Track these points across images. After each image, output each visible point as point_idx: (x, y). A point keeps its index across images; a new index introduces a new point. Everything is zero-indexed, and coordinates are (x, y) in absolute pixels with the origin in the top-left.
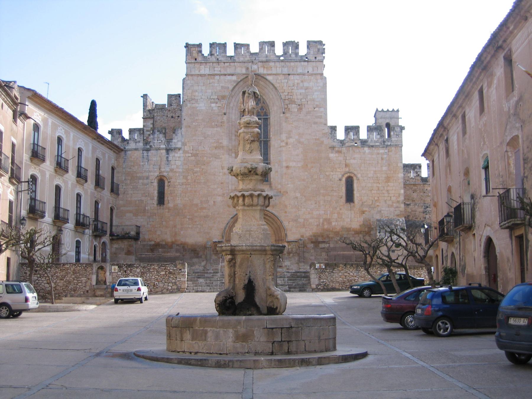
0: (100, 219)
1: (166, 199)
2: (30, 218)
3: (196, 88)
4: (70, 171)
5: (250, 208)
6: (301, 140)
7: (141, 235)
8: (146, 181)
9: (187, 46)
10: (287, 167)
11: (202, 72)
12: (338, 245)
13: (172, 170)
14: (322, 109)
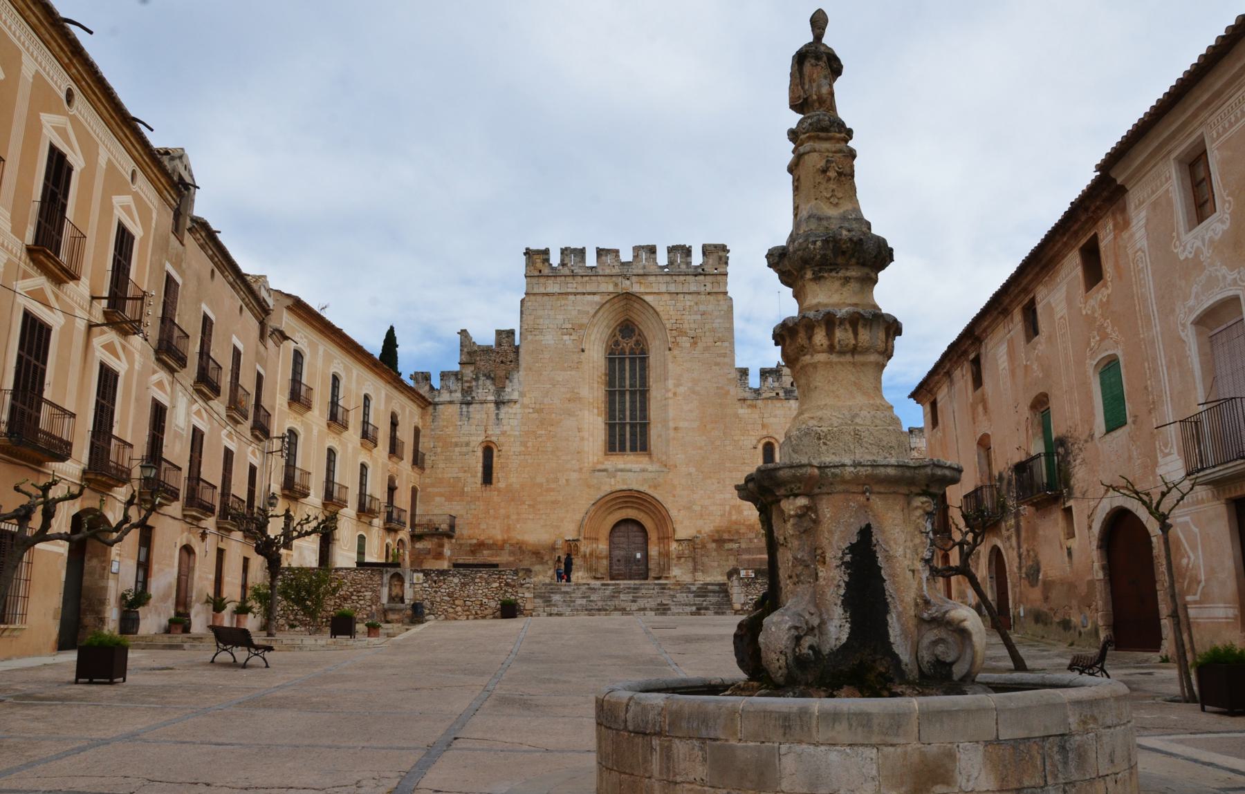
0: (396, 503)
1: (494, 475)
2: (284, 496)
3: (540, 313)
4: (351, 428)
5: (848, 358)
6: (697, 389)
7: (457, 530)
8: (464, 449)
9: (528, 253)
10: (676, 429)
11: (550, 290)
12: (752, 546)
13: (503, 433)
14: (726, 344)
